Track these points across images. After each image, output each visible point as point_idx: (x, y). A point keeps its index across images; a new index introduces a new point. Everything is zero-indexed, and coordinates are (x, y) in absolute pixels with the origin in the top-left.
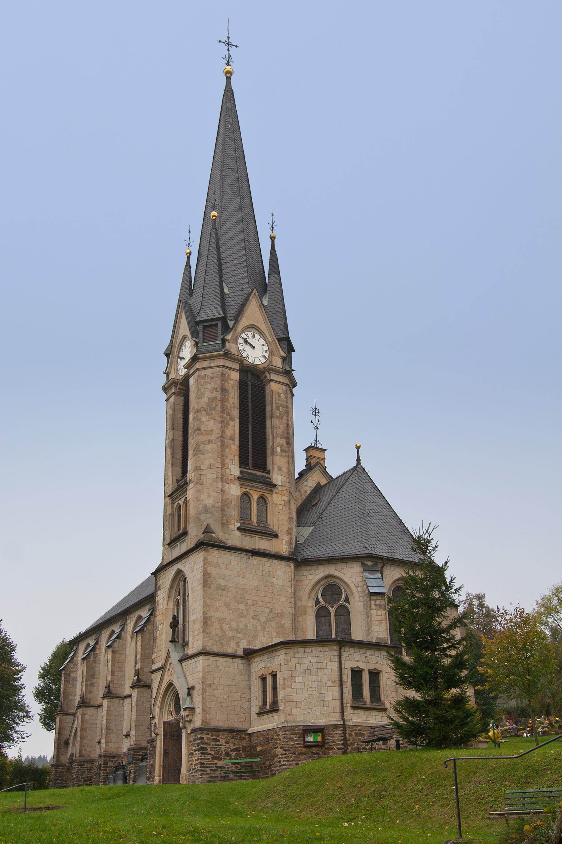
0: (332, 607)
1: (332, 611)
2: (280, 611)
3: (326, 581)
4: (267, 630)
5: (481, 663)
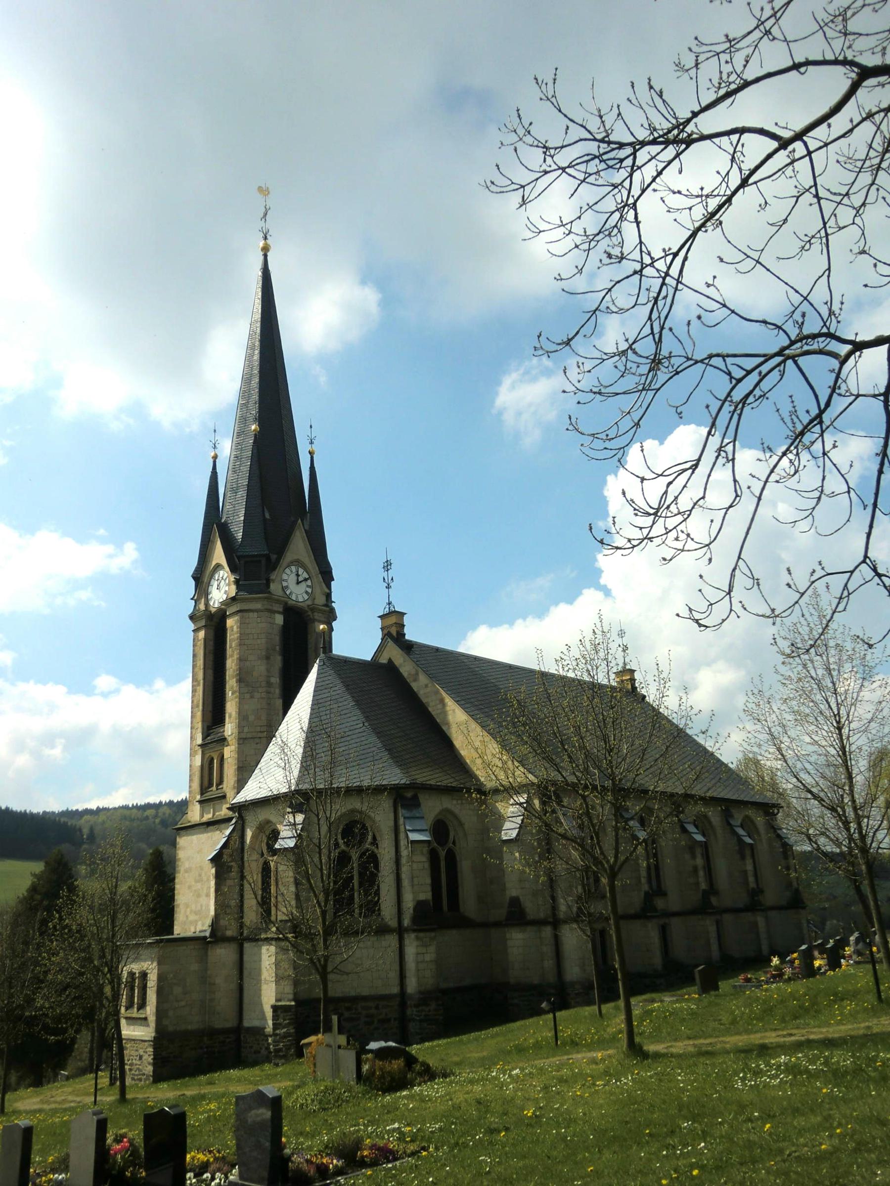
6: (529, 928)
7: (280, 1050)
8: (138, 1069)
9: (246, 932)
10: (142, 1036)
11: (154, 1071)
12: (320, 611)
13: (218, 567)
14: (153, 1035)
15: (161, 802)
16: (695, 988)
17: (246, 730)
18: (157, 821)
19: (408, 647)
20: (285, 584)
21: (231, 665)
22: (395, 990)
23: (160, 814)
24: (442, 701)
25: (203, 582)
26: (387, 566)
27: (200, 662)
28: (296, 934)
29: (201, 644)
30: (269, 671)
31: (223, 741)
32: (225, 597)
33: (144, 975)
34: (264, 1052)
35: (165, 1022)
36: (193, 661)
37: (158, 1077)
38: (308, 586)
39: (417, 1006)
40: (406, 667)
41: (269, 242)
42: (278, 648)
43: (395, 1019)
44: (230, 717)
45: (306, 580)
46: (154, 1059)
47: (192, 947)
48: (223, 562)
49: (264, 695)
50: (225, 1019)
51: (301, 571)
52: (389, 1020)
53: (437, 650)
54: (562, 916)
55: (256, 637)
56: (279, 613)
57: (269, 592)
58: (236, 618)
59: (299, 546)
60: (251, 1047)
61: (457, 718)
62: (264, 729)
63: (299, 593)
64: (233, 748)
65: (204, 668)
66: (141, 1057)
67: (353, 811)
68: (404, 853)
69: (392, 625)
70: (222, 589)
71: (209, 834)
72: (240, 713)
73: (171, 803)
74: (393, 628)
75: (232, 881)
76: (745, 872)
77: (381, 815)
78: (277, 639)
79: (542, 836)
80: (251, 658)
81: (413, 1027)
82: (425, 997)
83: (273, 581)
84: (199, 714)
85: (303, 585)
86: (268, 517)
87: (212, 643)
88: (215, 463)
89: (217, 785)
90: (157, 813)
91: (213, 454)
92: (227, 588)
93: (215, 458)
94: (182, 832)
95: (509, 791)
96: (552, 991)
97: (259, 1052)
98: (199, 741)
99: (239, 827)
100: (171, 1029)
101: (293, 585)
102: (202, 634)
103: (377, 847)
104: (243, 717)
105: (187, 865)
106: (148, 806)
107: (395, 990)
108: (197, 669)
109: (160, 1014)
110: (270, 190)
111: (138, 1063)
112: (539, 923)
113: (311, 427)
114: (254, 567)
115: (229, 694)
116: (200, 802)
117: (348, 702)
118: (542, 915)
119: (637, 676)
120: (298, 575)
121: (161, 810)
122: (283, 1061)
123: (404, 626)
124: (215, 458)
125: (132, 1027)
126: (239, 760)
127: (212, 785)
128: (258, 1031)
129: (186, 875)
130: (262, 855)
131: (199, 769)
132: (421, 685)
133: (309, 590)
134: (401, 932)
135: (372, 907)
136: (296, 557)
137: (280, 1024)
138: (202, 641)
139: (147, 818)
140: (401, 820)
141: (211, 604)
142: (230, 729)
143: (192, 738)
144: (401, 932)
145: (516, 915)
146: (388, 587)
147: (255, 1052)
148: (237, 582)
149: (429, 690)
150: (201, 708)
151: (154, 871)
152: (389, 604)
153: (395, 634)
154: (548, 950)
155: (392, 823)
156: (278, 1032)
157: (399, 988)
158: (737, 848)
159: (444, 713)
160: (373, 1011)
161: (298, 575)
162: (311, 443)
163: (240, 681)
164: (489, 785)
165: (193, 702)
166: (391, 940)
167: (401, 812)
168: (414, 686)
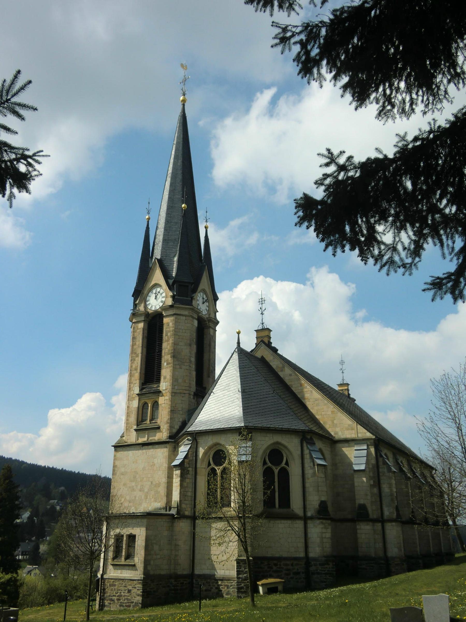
0: (276, 469)
1: (276, 471)
2: (157, 482)
3: (215, 447)
4: (148, 497)
5: (372, 238)
7: (242, 588)
8: (127, 599)
10: (131, 577)
11: (142, 600)
13: (156, 285)
17: (176, 387)
22: (302, 555)
25: (143, 293)
27: (139, 342)
31: (158, 393)
33: (132, 538)
34: (214, 590)
35: (149, 568)
37: (145, 605)
40: (275, 364)
46: (143, 592)
47: (164, 520)
48: (162, 281)
49: (187, 367)
50: (183, 568)
52: (298, 573)
54: (385, 517)
55: (184, 331)
56: (196, 319)
58: (172, 318)
62: (187, 388)
64: (167, 398)
65: (142, 347)
66: (129, 591)
70: (159, 299)
71: (144, 451)
77: (292, 444)
78: (195, 335)
87: (146, 331)
88: (148, 222)
89: (150, 420)
92: (164, 299)
97: (210, 591)
98: (137, 390)
100: (152, 573)
102: (141, 325)
104: (175, 380)
105: (123, 470)
107: (302, 555)
108: (135, 347)
109: (146, 562)
111: (127, 594)
112: (374, 521)
115: (164, 364)
116: (135, 430)
120: (203, 298)
125: (119, 571)
127: (146, 420)
128: (211, 579)
129: (122, 477)
130: (209, 464)
131: (136, 409)
134: (305, 519)
136: (203, 288)
137: (242, 571)
138: (142, 330)
141: (149, 307)
143: (130, 389)
144: (305, 519)
145: (362, 514)
146: (262, 314)
148: (173, 297)
153: (267, 342)
155: (299, 452)
156: (241, 576)
157: (304, 553)
159: (302, 392)
161: (203, 298)
163: (174, 356)
164: (337, 437)
165: (131, 367)
166: (300, 524)
167: (305, 444)
168: (281, 374)
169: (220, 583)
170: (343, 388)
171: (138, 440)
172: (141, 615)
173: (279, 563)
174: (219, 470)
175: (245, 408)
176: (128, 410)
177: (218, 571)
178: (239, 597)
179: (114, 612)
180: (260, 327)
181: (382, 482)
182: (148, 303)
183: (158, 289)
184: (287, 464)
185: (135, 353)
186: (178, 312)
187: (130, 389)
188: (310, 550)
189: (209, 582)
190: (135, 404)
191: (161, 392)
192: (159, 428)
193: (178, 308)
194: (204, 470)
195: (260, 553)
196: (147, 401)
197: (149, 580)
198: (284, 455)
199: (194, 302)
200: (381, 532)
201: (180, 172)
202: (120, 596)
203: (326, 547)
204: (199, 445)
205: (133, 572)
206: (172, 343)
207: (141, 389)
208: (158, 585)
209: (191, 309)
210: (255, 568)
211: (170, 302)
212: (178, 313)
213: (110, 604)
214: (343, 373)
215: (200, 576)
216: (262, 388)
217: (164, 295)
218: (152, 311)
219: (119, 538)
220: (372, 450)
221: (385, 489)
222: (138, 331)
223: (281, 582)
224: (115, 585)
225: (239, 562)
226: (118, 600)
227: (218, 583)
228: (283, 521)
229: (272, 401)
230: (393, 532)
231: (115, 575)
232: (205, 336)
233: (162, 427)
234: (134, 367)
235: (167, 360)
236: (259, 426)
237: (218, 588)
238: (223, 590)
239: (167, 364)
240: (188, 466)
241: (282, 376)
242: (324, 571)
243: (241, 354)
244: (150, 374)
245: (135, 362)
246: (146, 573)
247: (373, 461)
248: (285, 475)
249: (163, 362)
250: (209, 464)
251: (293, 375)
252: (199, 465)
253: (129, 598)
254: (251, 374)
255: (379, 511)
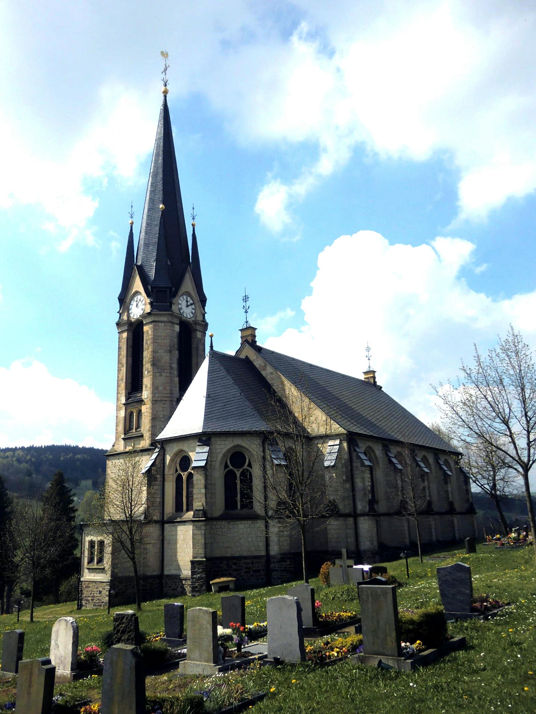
1: (238, 474)
6: (340, 518)
7: (196, 587)
8: (99, 599)
9: (165, 518)
10: (101, 579)
12: (200, 325)
13: (137, 293)
14: (110, 578)
15: (16, 448)
16: (465, 550)
18: (14, 459)
19: (259, 350)
20: (180, 306)
21: (147, 355)
22: (263, 553)
23: (16, 455)
24: (282, 383)
25: (126, 302)
26: (246, 299)
27: (124, 352)
28: (206, 519)
29: (124, 341)
30: (170, 360)
31: (141, 402)
32: (142, 312)
34: (179, 589)
36: (119, 352)
38: (193, 309)
39: (279, 562)
40: (258, 362)
41: (168, 87)
42: (176, 346)
43: (263, 570)
44: (146, 387)
45: (192, 304)
48: (141, 289)
49: (168, 374)
50: (152, 569)
51: (189, 299)
52: (259, 571)
53: (273, 352)
54: (359, 512)
56: (177, 324)
57: (172, 311)
58: (151, 326)
59: (188, 284)
60: (171, 587)
61: (292, 392)
63: (188, 312)
64: (148, 406)
65: (127, 356)
66: (100, 592)
67: (235, 447)
68: (269, 472)
69: (249, 336)
70: (140, 306)
72: (153, 384)
73: (23, 449)
74: (249, 337)
75: (157, 487)
76: (447, 491)
77: (253, 448)
78: (176, 340)
79: (349, 463)
80: (160, 351)
81: (274, 574)
82: (284, 557)
83: (174, 304)
84: (123, 385)
85: (190, 307)
86: (167, 263)
87: (131, 341)
88: (132, 227)
89: (136, 429)
90: (14, 454)
91: (130, 222)
92: (144, 307)
93: (132, 224)
94: (110, 458)
95: (326, 437)
96: (353, 555)
97: (176, 590)
98: (123, 400)
99: (162, 454)
101: (184, 307)
102: (125, 335)
103: (251, 468)
104: (155, 388)
106: (8, 450)
107: (263, 553)
108: (121, 357)
109: (114, 566)
110: (169, 54)
111: (99, 595)
113: (193, 208)
114: (162, 295)
115: (145, 373)
116: (123, 439)
117: (230, 381)
118: (347, 512)
119: (376, 375)
120: (187, 301)
121: (17, 453)
122: (198, 594)
123: (255, 336)
124: (132, 224)
125: (93, 574)
126: (153, 414)
127: (133, 429)
128: (177, 578)
130: (177, 471)
131: (123, 419)
132: (268, 372)
133: (194, 311)
135: (250, 505)
139: (7, 457)
140: (268, 452)
142: (146, 394)
144: (266, 518)
145: (334, 511)
146: (246, 312)
147: (173, 590)
148: (151, 304)
149: (273, 376)
150: (124, 380)
151: (57, 485)
152: (247, 322)
153: (250, 341)
154: (351, 532)
156: (195, 576)
158: (443, 477)
160: (251, 565)
162: (193, 219)
163: (153, 365)
165: (118, 377)
168: (263, 373)
169: (184, 582)
170: (369, 376)
171: (126, 448)
172: (94, 614)
173: (238, 562)
174: (184, 475)
175: (207, 414)
176: (117, 420)
177: (183, 571)
178: (194, 596)
179: (90, 611)
180: (245, 326)
181: (356, 476)
182: (130, 312)
183: (139, 297)
184: (250, 465)
185: (121, 363)
186: (157, 319)
187: (117, 399)
188: (271, 548)
189: (175, 582)
190: (122, 413)
191: (143, 400)
192: (142, 436)
193: (156, 315)
194: (171, 476)
195: (218, 553)
196: (132, 410)
197: (114, 582)
198: (247, 457)
199: (174, 308)
200: (353, 526)
201: (160, 170)
202: (93, 597)
203: (283, 545)
204: (166, 452)
205: (104, 575)
206: (151, 351)
207: (128, 398)
208: (126, 585)
209: (169, 314)
210: (210, 567)
211: (148, 309)
212: (157, 319)
213: (86, 603)
214: (369, 359)
215: (168, 576)
216: (229, 392)
217: (144, 302)
218: (134, 320)
219: (92, 543)
220: (345, 445)
221: (359, 483)
222: (123, 341)
223: (231, 580)
224: (89, 587)
225: (193, 562)
226: (92, 600)
227: (182, 582)
228: (243, 522)
229: (238, 404)
230: (366, 525)
231: (90, 577)
232: (193, 340)
233: (145, 435)
234: (120, 377)
235: (148, 369)
236: (218, 430)
237: (182, 587)
238: (186, 589)
239: (148, 373)
240: (155, 473)
241: (264, 375)
242: (281, 568)
243: (213, 358)
244: (134, 384)
245: (121, 372)
246: (113, 575)
247: (346, 456)
248: (247, 478)
249: (144, 371)
250: (177, 471)
251: (274, 373)
252: (166, 472)
253: (100, 598)
254: (220, 377)
255: (352, 506)
